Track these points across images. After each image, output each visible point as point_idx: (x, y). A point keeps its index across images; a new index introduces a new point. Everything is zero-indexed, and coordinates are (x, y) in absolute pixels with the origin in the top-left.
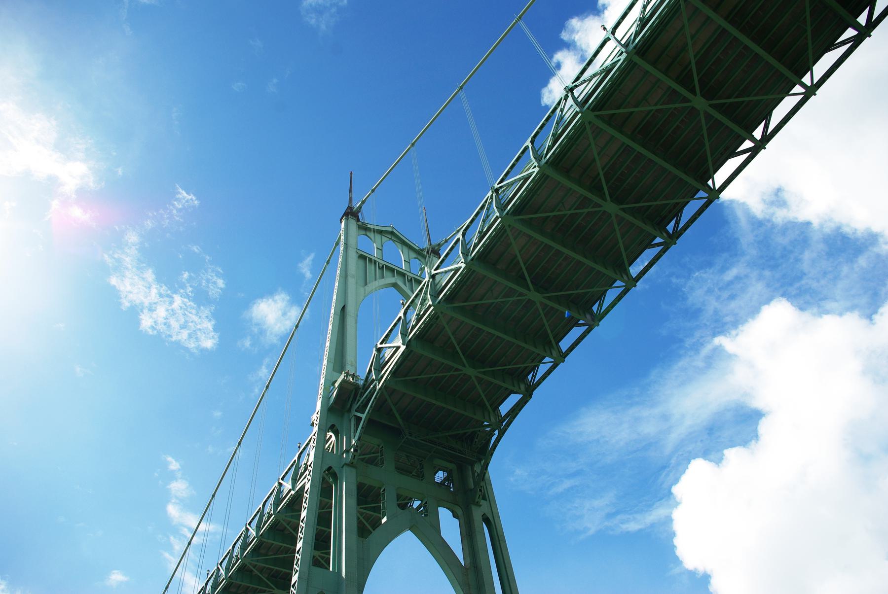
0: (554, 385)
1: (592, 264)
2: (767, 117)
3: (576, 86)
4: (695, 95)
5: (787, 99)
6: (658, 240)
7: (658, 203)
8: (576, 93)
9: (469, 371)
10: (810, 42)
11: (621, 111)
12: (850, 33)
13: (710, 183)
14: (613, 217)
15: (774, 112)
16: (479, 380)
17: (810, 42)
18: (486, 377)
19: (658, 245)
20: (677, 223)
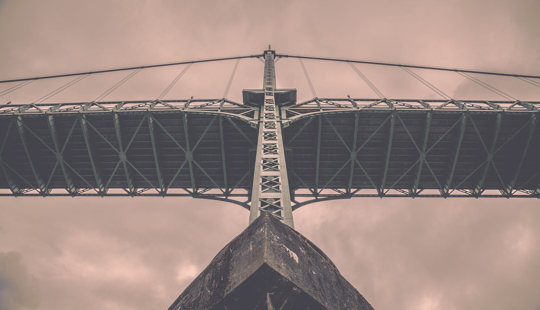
0: (88, 202)
1: (94, 170)
2: (359, 189)
3: (160, 103)
4: (356, 151)
5: (64, 189)
6: (128, 190)
7: (143, 176)
8: (225, 103)
9: (59, 157)
10: (242, 179)
11: (95, 129)
12: (191, 190)
13: (230, 189)
14: (185, 161)
15: (300, 189)
16: (121, 165)
17: (242, 179)
18: (63, 169)
19: (127, 191)
20: (355, 192)
